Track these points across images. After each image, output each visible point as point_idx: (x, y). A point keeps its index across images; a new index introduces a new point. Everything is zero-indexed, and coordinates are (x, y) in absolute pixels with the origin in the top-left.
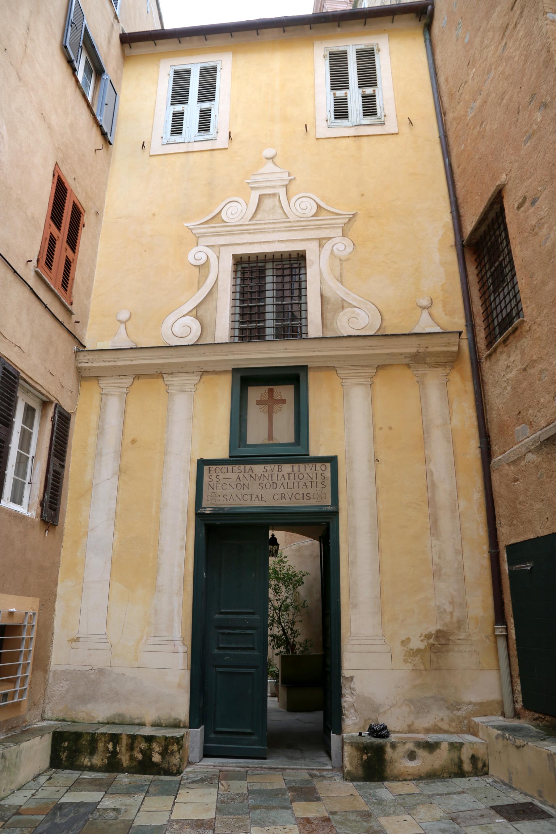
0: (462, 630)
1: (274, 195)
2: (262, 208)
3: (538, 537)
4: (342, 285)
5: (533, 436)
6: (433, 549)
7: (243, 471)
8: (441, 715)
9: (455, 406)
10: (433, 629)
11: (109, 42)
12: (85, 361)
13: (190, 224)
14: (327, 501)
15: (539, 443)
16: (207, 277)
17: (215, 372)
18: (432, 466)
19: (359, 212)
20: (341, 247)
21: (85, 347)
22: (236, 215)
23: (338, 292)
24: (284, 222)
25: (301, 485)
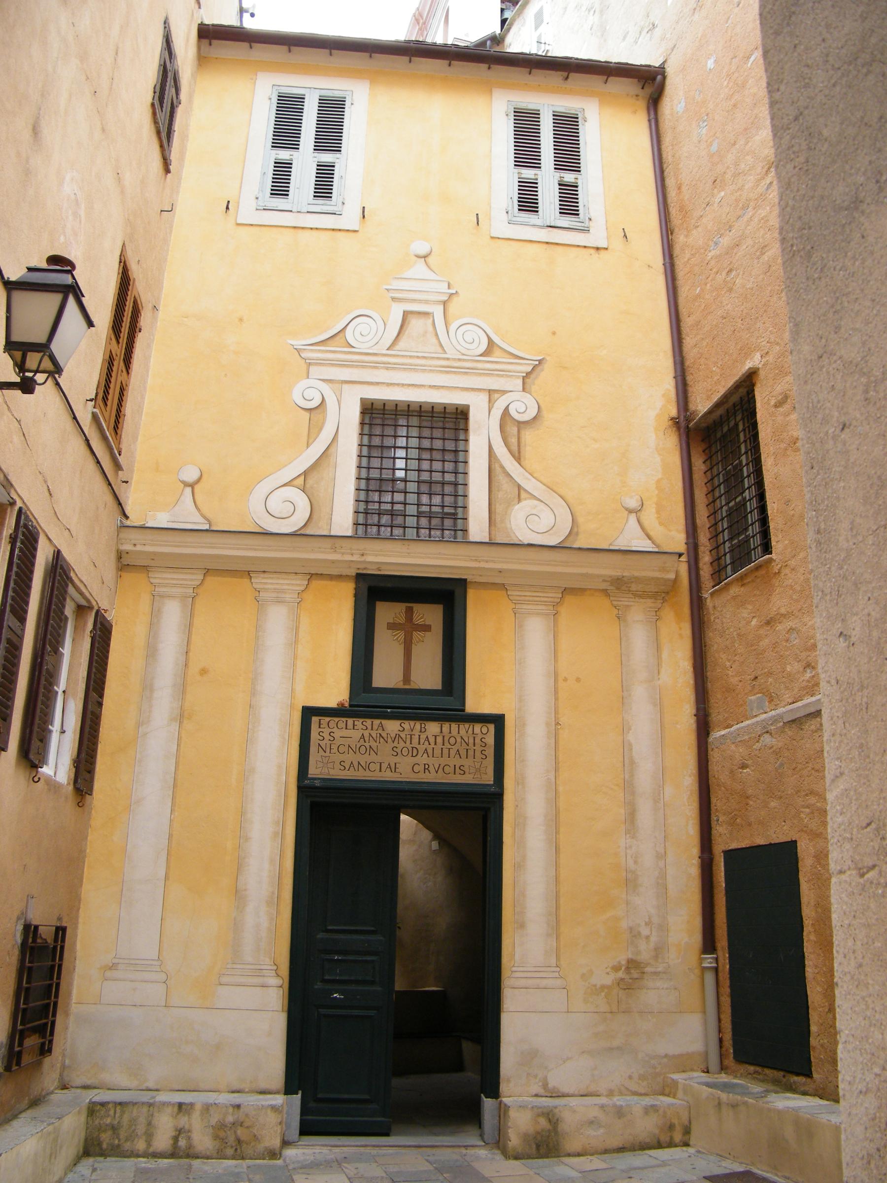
0: (660, 960)
1: (426, 314)
3: (771, 844)
5: (773, 713)
7: (369, 727)
9: (665, 655)
12: (133, 543)
13: (298, 343)
14: (488, 778)
15: (781, 724)
17: (331, 577)
18: (630, 737)
19: (548, 358)
22: (370, 336)
24: (438, 358)
25: (453, 752)
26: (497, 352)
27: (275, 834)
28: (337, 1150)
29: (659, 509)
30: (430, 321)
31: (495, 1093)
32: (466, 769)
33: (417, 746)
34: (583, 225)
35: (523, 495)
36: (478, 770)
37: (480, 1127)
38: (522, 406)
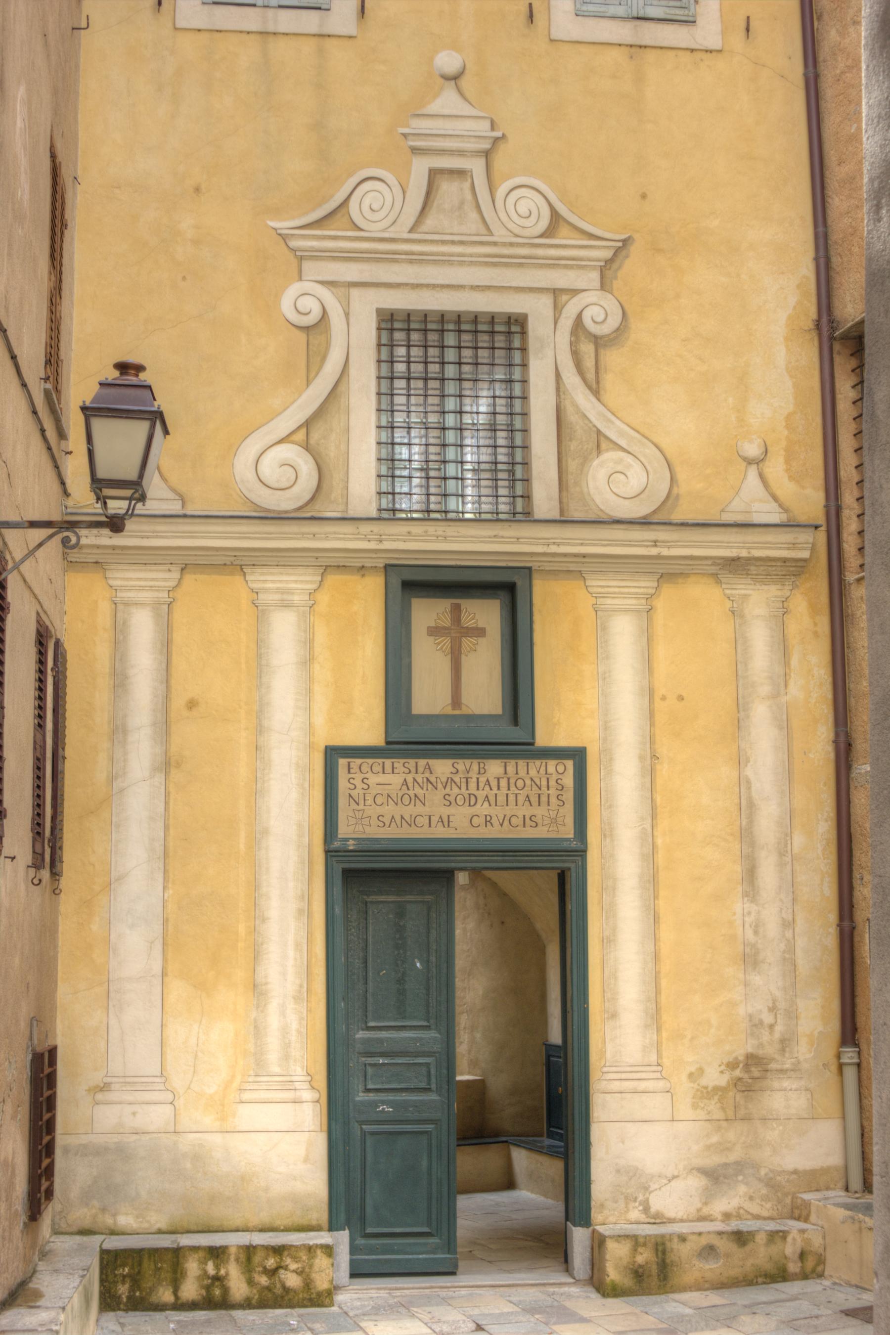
0: (787, 1055)
2: (435, 204)
7: (413, 770)
9: (794, 661)
10: (740, 1053)
13: (283, 225)
14: (568, 831)
16: (324, 358)
18: (749, 772)
19: (636, 236)
24: (482, 243)
25: (521, 799)
26: (564, 230)
27: (300, 911)
28: (398, 1293)
29: (789, 457)
30: (467, 185)
31: (585, 1220)
32: (538, 819)
33: (476, 793)
34: (686, 12)
35: (604, 445)
36: (554, 821)
37: (566, 1261)
38: (598, 310)
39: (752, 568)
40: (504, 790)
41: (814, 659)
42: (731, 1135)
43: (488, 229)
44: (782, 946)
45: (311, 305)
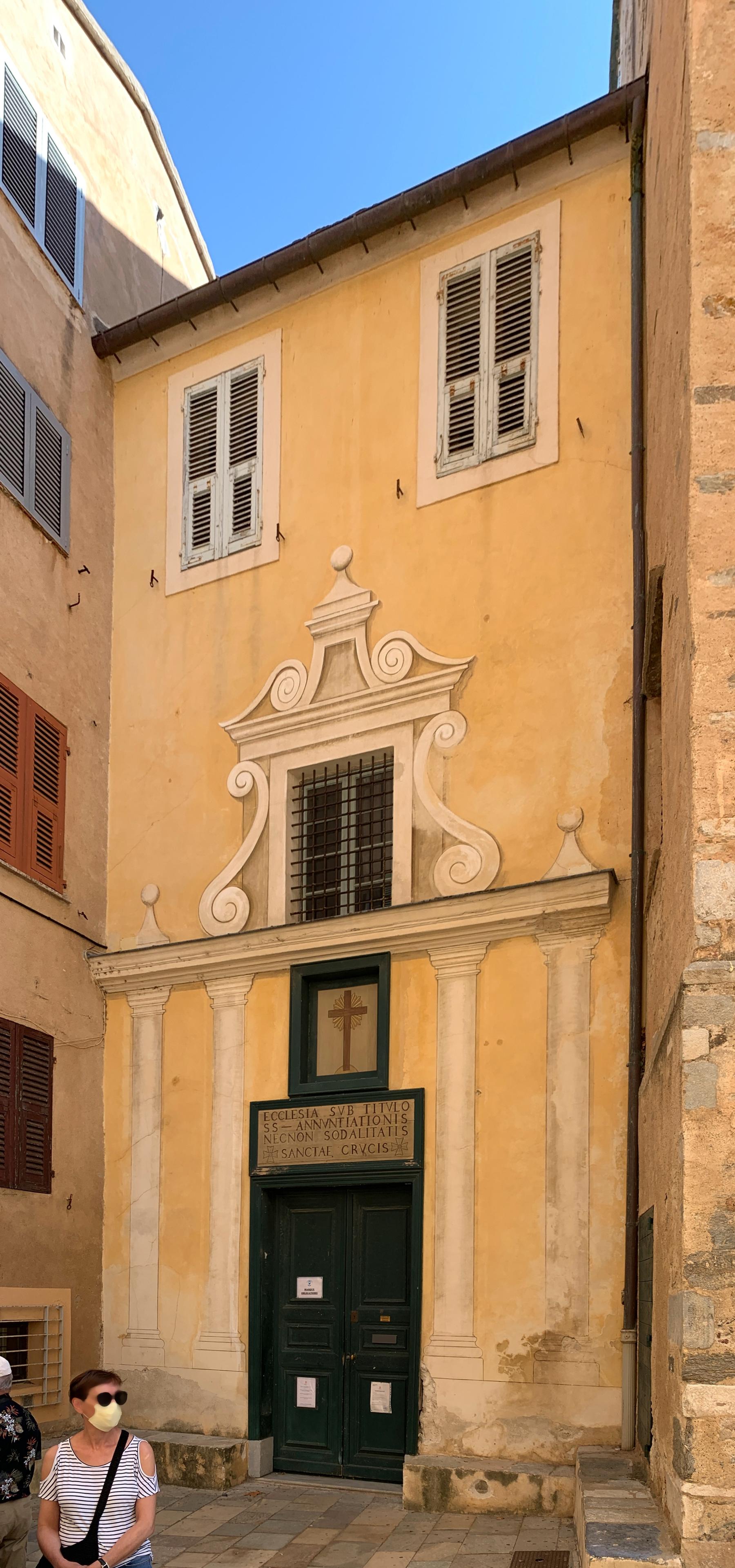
0: (579, 1333)
1: (347, 643)
4: (445, 804)
6: (549, 1220)
7: (305, 1115)
8: (542, 1441)
9: (599, 1001)
10: (540, 1331)
11: (66, 366)
16: (254, 817)
18: (555, 1098)
20: (446, 730)
21: (106, 948)
23: (437, 820)
25: (377, 1131)
36: (400, 1147)
39: (564, 923)
40: (365, 1126)
41: (616, 996)
42: (529, 1395)
43: (366, 684)
44: (578, 1243)
45: (246, 779)
